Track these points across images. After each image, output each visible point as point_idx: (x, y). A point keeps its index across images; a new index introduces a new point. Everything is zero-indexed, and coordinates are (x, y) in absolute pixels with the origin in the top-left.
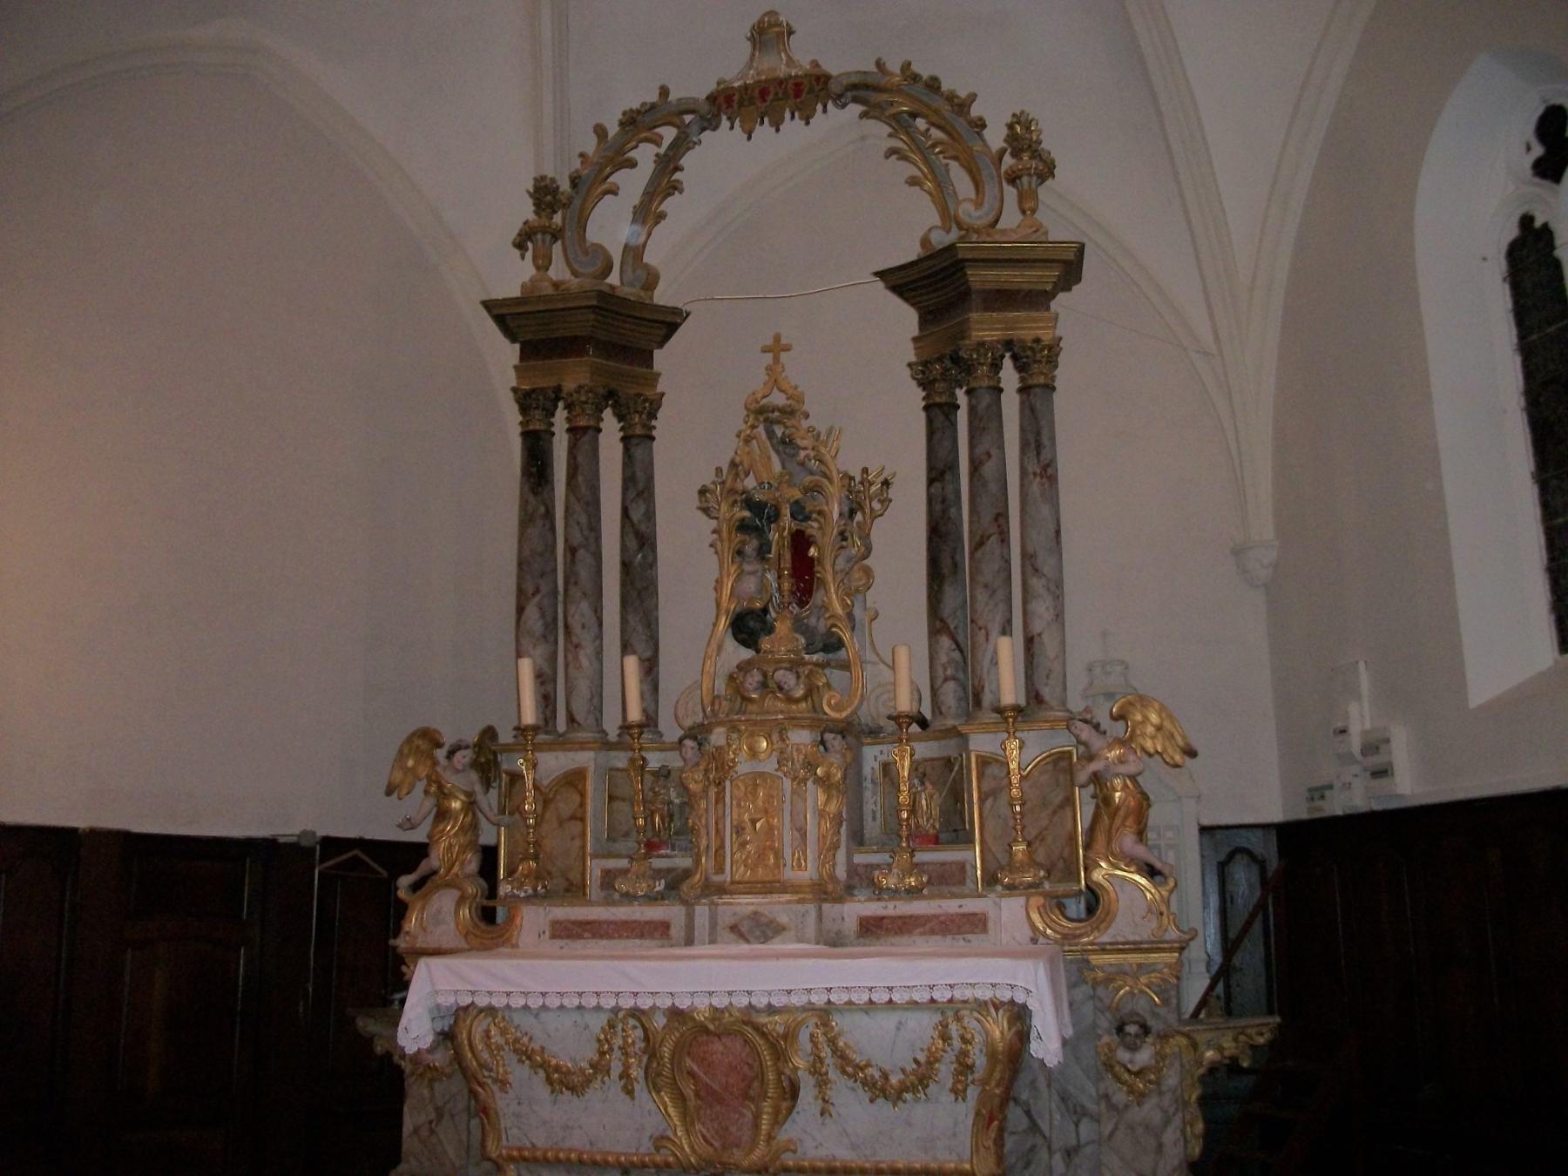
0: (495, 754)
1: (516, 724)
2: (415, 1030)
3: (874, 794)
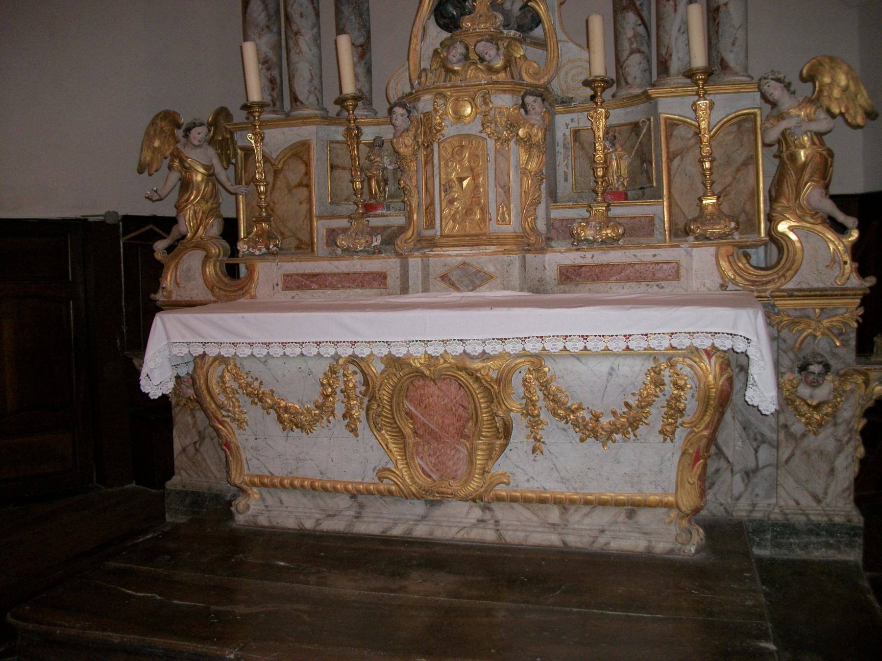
0: (232, 133)
2: (157, 376)
3: (566, 157)
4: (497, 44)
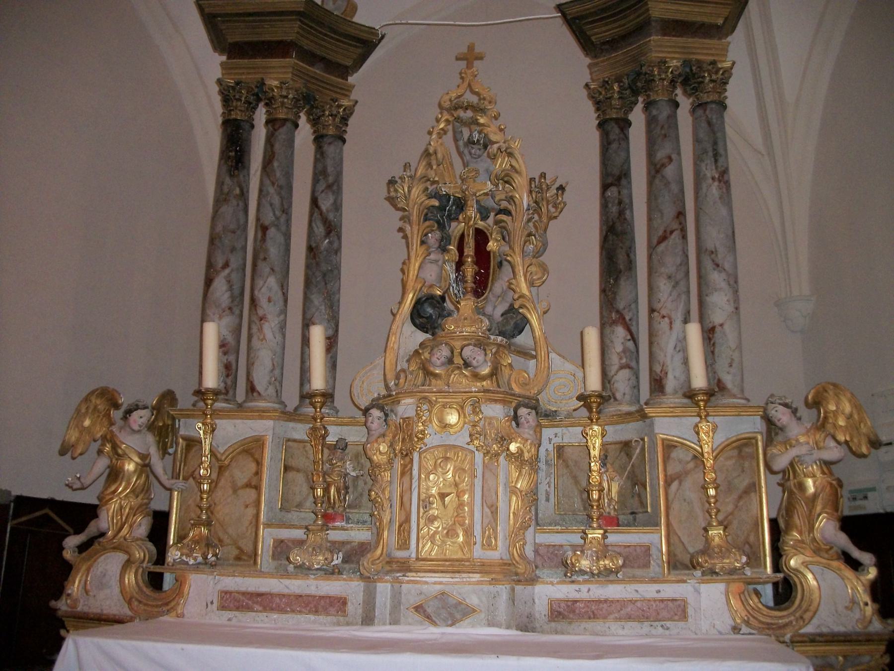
1: (196, 387)
3: (548, 475)
4: (485, 350)
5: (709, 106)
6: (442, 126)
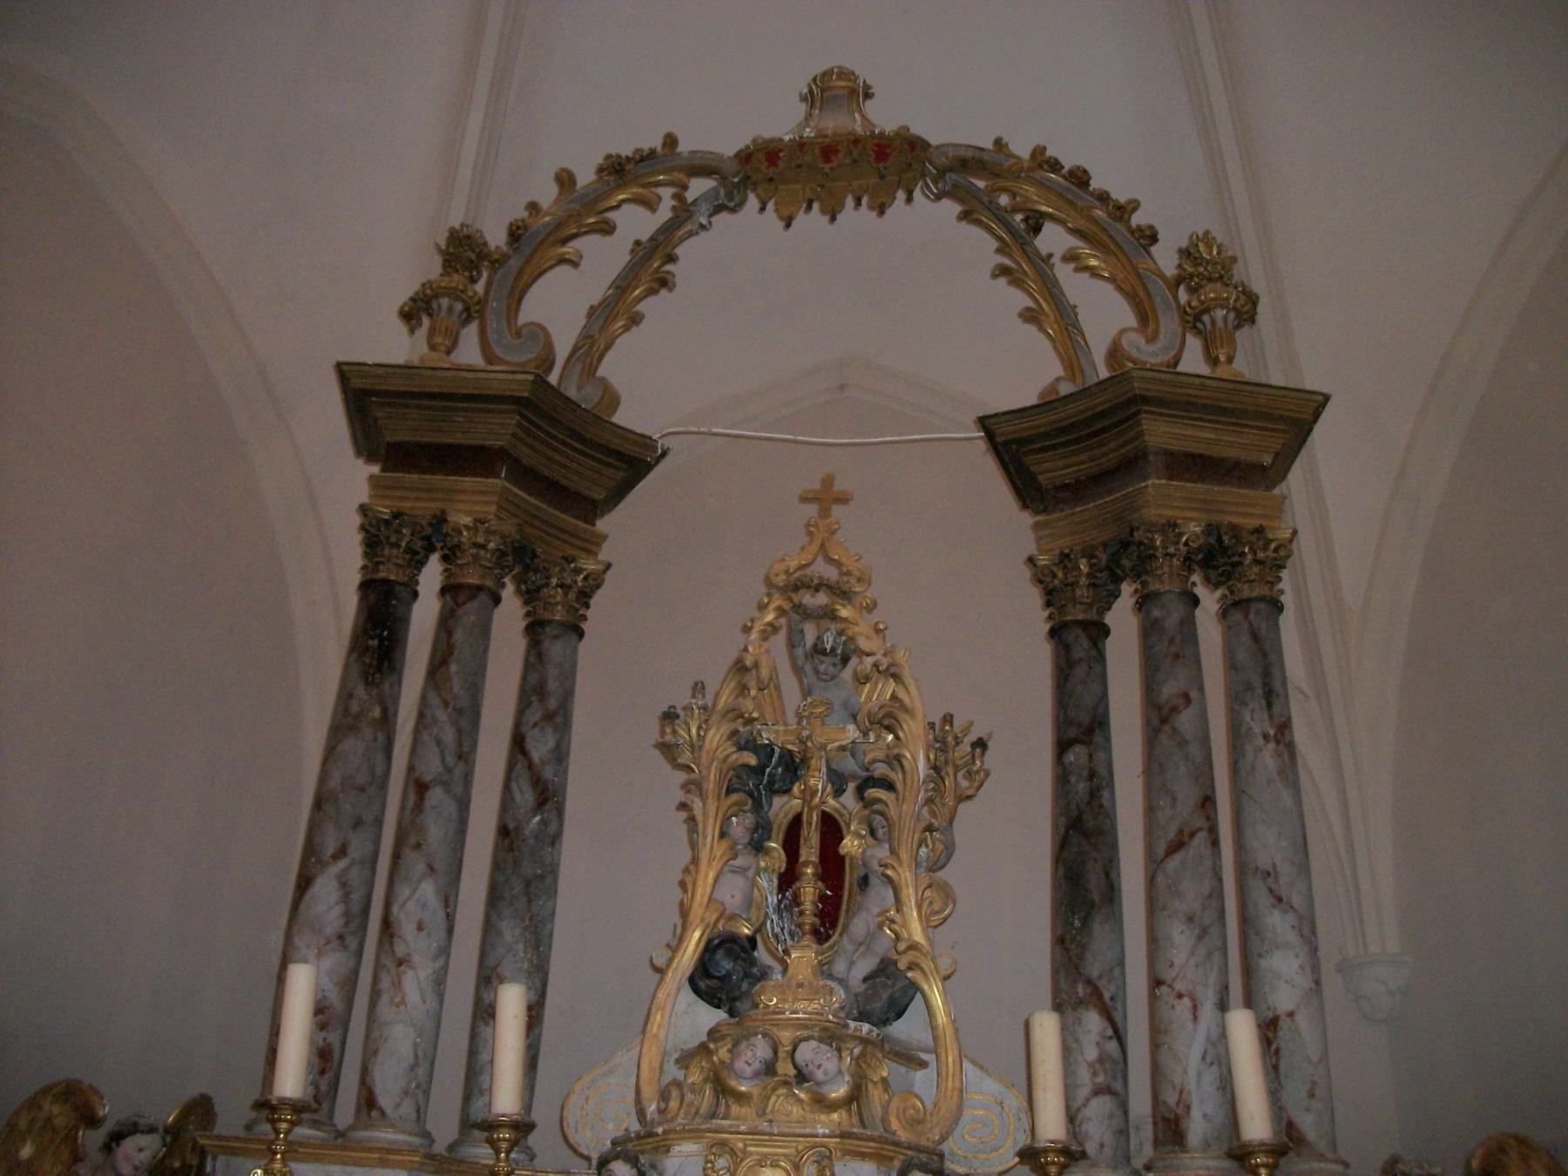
0: (203, 1153)
4: (839, 1050)
5: (1254, 607)
6: (770, 617)
